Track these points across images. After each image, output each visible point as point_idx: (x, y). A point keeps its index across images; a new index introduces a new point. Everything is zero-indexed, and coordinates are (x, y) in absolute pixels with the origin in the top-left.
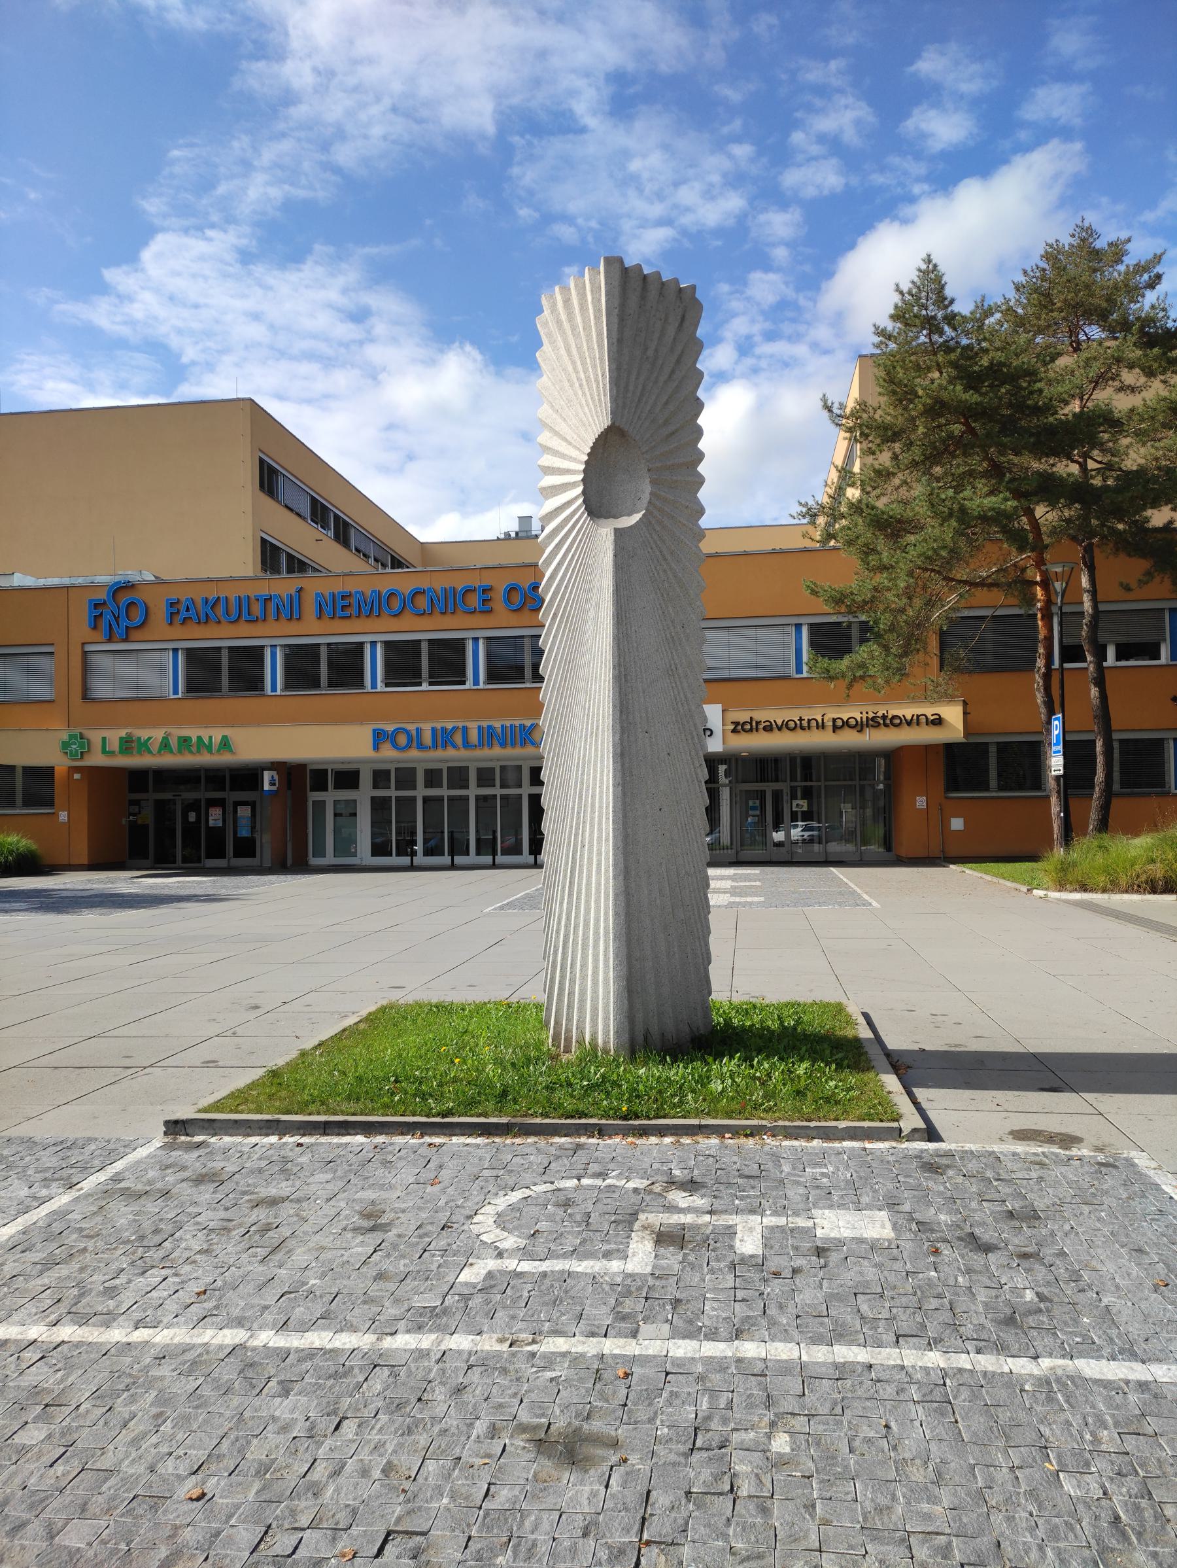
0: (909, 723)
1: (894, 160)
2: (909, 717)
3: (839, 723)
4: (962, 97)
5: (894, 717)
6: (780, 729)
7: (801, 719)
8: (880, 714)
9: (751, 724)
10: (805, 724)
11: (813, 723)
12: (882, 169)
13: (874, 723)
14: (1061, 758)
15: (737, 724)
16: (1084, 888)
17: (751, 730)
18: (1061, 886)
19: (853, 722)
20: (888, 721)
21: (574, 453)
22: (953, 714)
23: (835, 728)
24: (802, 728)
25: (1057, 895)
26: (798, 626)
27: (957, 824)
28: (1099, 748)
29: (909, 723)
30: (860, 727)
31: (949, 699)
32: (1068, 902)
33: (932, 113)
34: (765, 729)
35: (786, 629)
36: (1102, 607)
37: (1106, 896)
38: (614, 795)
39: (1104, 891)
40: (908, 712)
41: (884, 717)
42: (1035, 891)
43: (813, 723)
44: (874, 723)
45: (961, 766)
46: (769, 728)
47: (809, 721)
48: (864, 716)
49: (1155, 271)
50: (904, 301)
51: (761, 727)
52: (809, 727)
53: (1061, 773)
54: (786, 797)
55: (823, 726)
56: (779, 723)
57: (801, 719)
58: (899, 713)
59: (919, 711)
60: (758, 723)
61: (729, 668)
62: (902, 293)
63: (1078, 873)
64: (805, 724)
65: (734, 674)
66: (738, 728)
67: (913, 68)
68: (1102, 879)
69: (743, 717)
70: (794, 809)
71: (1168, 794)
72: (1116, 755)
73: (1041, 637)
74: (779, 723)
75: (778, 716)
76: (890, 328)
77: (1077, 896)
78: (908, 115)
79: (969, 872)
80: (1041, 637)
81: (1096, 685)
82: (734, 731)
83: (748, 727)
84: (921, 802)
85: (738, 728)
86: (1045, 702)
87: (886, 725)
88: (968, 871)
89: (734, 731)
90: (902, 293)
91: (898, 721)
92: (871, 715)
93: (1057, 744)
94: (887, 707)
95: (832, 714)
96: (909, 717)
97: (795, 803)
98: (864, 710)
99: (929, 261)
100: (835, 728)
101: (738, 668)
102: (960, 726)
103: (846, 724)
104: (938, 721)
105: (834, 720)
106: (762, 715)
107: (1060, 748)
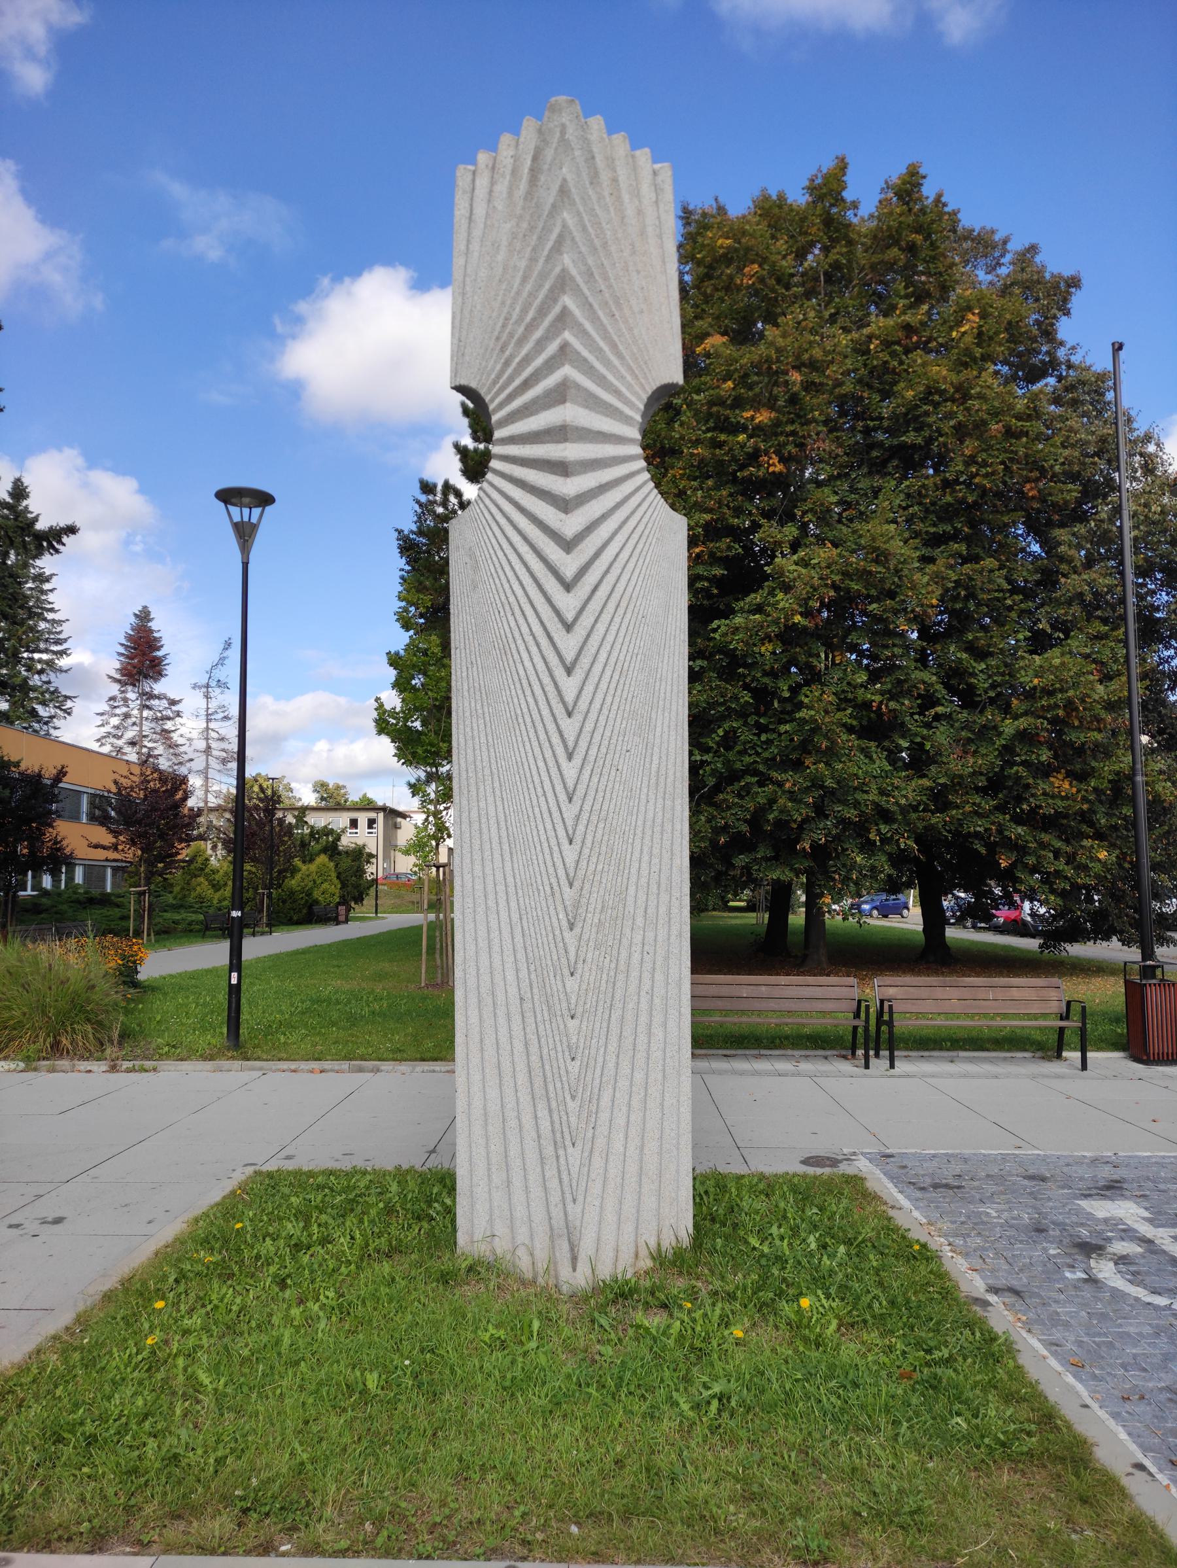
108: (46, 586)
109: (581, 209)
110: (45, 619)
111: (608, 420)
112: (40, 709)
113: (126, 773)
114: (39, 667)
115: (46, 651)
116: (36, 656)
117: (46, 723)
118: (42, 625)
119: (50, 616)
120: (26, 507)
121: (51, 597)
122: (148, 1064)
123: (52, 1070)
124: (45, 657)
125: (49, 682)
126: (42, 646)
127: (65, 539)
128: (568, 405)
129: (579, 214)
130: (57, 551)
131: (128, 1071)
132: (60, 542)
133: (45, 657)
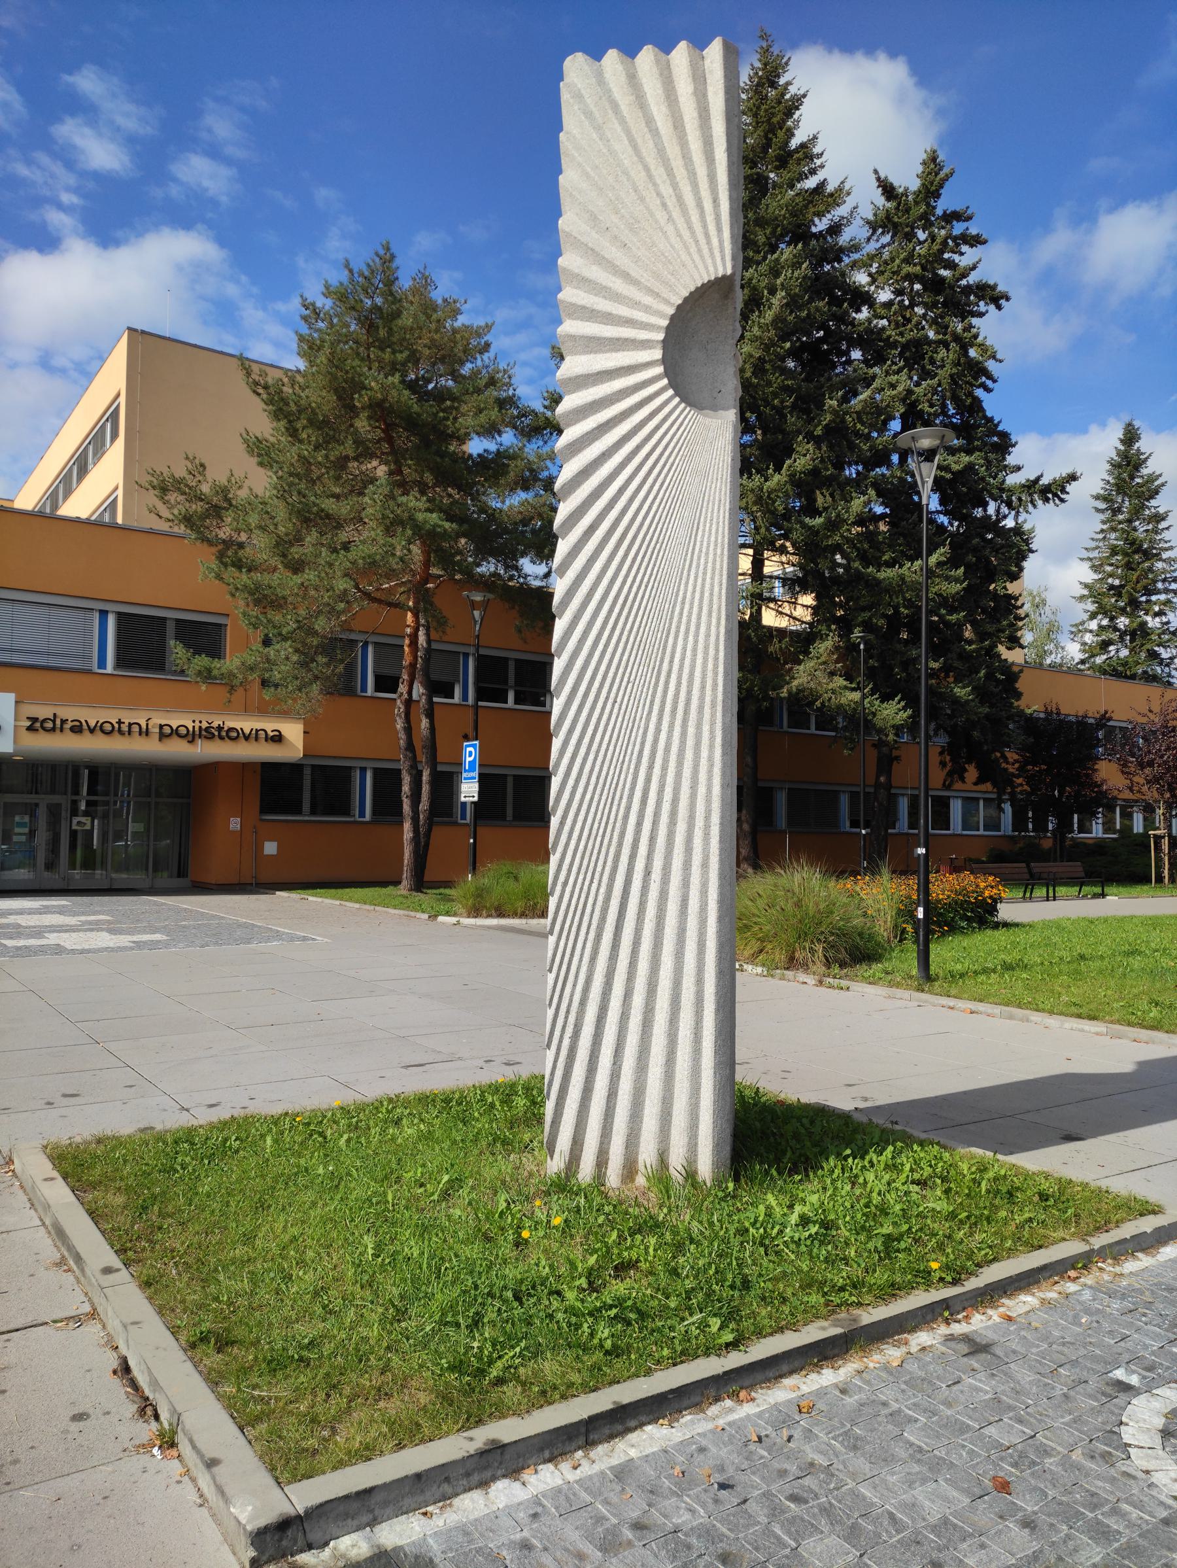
0: (247, 738)
1: (43, 158)
2: (247, 731)
3: (167, 730)
4: (118, 129)
5: (231, 729)
6: (92, 731)
7: (120, 722)
8: (215, 725)
9: (54, 721)
10: (125, 728)
11: (136, 728)
12: (29, 162)
13: (208, 734)
14: (477, 785)
15: (34, 720)
16: (501, 915)
17: (53, 729)
18: (475, 912)
19: (183, 731)
20: (224, 734)
21: (711, 269)
22: (293, 732)
23: (162, 736)
24: (120, 732)
25: (472, 921)
26: (104, 613)
27: (270, 848)
28: (406, 780)
29: (247, 738)
30: (191, 737)
31: (285, 714)
32: (489, 927)
33: (87, 131)
34: (72, 729)
35: (88, 615)
36: (434, 646)
37: (524, 921)
38: (723, 800)
39: (523, 915)
40: (247, 725)
41: (220, 728)
42: (441, 919)
43: (136, 728)
44: (208, 734)
45: (277, 787)
46: (77, 729)
47: (130, 725)
48: (197, 724)
49: (486, 338)
50: (352, 281)
51: (68, 726)
52: (130, 732)
53: (476, 799)
54: (65, 814)
55: (147, 733)
56: (92, 724)
57: (120, 722)
58: (237, 725)
59: (258, 725)
60: (63, 722)
61: (11, 650)
62: (351, 271)
63: (493, 899)
64: (125, 728)
65: (53, 662)
66: (35, 725)
67: (70, 79)
68: (520, 905)
69: (43, 712)
70: (74, 827)
71: (456, 823)
72: (425, 789)
73: (406, 663)
74: (92, 724)
75: (92, 717)
76: (319, 304)
77: (494, 922)
78: (60, 120)
79: (315, 900)
80: (406, 663)
81: (427, 716)
82: (29, 729)
83: (49, 725)
84: (235, 824)
85: (35, 725)
86: (405, 728)
87: (221, 738)
88: (311, 898)
89: (29, 729)
90: (351, 271)
91: (235, 734)
92: (205, 725)
93: (472, 769)
94: (224, 718)
95: (158, 719)
96: (247, 731)
97: (75, 820)
98: (197, 717)
99: (388, 249)
100: (162, 736)
101: (63, 655)
102: (300, 745)
103: (175, 732)
104: (278, 738)
105: (161, 727)
106: (71, 713)
107: (476, 774)
108: (1163, 525)
109: (580, 159)
110: (1161, 559)
111: (600, 356)
112: (1161, 650)
113: (1145, 710)
114: (1157, 609)
115: (1166, 591)
116: (1154, 598)
117: (1168, 665)
118: (1159, 565)
119: (1165, 555)
120: (1138, 450)
121: (1166, 535)
122: (844, 983)
123: (782, 978)
124: (1163, 597)
125: (1168, 623)
126: (1160, 585)
127: (1068, 488)
128: (568, 359)
129: (580, 165)
130: (1062, 501)
131: (831, 987)
132: (1064, 491)
133: (1163, 597)
